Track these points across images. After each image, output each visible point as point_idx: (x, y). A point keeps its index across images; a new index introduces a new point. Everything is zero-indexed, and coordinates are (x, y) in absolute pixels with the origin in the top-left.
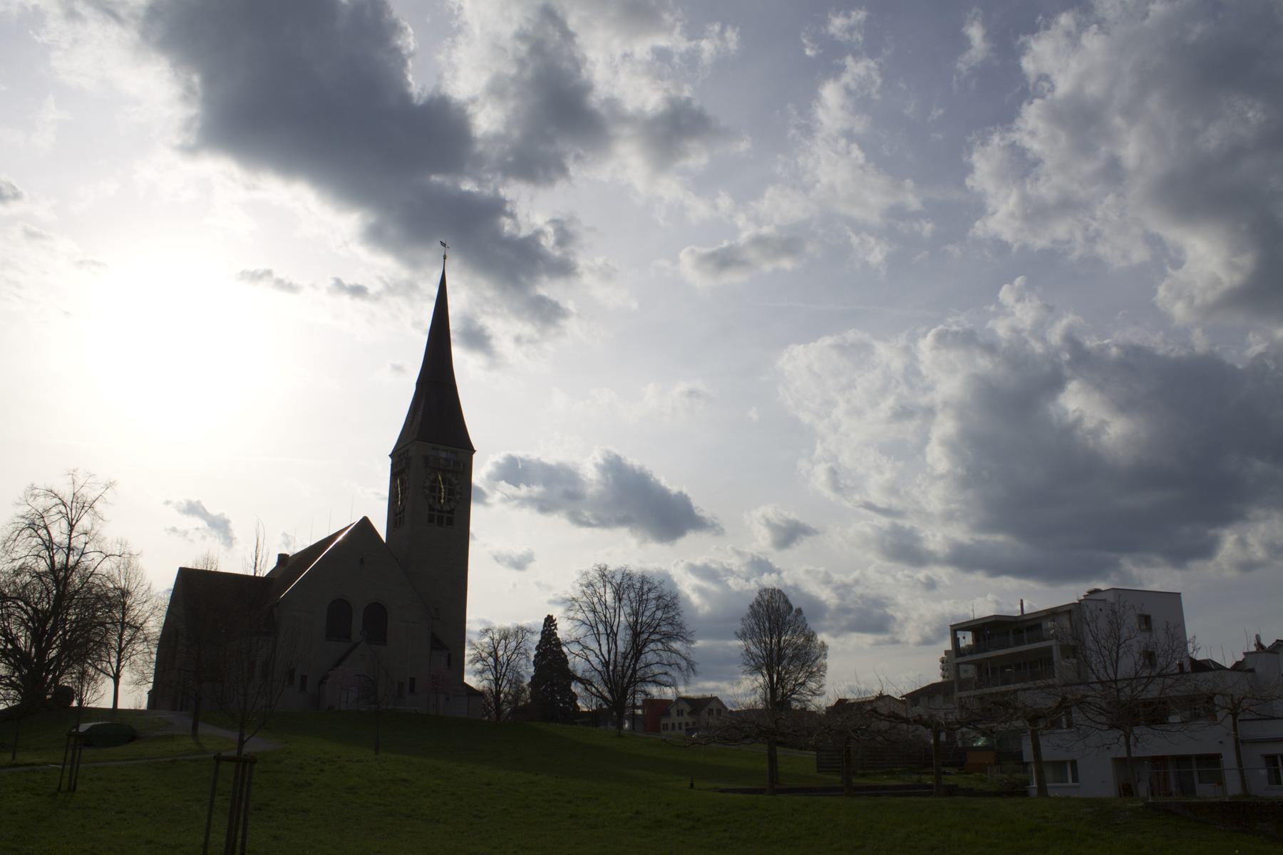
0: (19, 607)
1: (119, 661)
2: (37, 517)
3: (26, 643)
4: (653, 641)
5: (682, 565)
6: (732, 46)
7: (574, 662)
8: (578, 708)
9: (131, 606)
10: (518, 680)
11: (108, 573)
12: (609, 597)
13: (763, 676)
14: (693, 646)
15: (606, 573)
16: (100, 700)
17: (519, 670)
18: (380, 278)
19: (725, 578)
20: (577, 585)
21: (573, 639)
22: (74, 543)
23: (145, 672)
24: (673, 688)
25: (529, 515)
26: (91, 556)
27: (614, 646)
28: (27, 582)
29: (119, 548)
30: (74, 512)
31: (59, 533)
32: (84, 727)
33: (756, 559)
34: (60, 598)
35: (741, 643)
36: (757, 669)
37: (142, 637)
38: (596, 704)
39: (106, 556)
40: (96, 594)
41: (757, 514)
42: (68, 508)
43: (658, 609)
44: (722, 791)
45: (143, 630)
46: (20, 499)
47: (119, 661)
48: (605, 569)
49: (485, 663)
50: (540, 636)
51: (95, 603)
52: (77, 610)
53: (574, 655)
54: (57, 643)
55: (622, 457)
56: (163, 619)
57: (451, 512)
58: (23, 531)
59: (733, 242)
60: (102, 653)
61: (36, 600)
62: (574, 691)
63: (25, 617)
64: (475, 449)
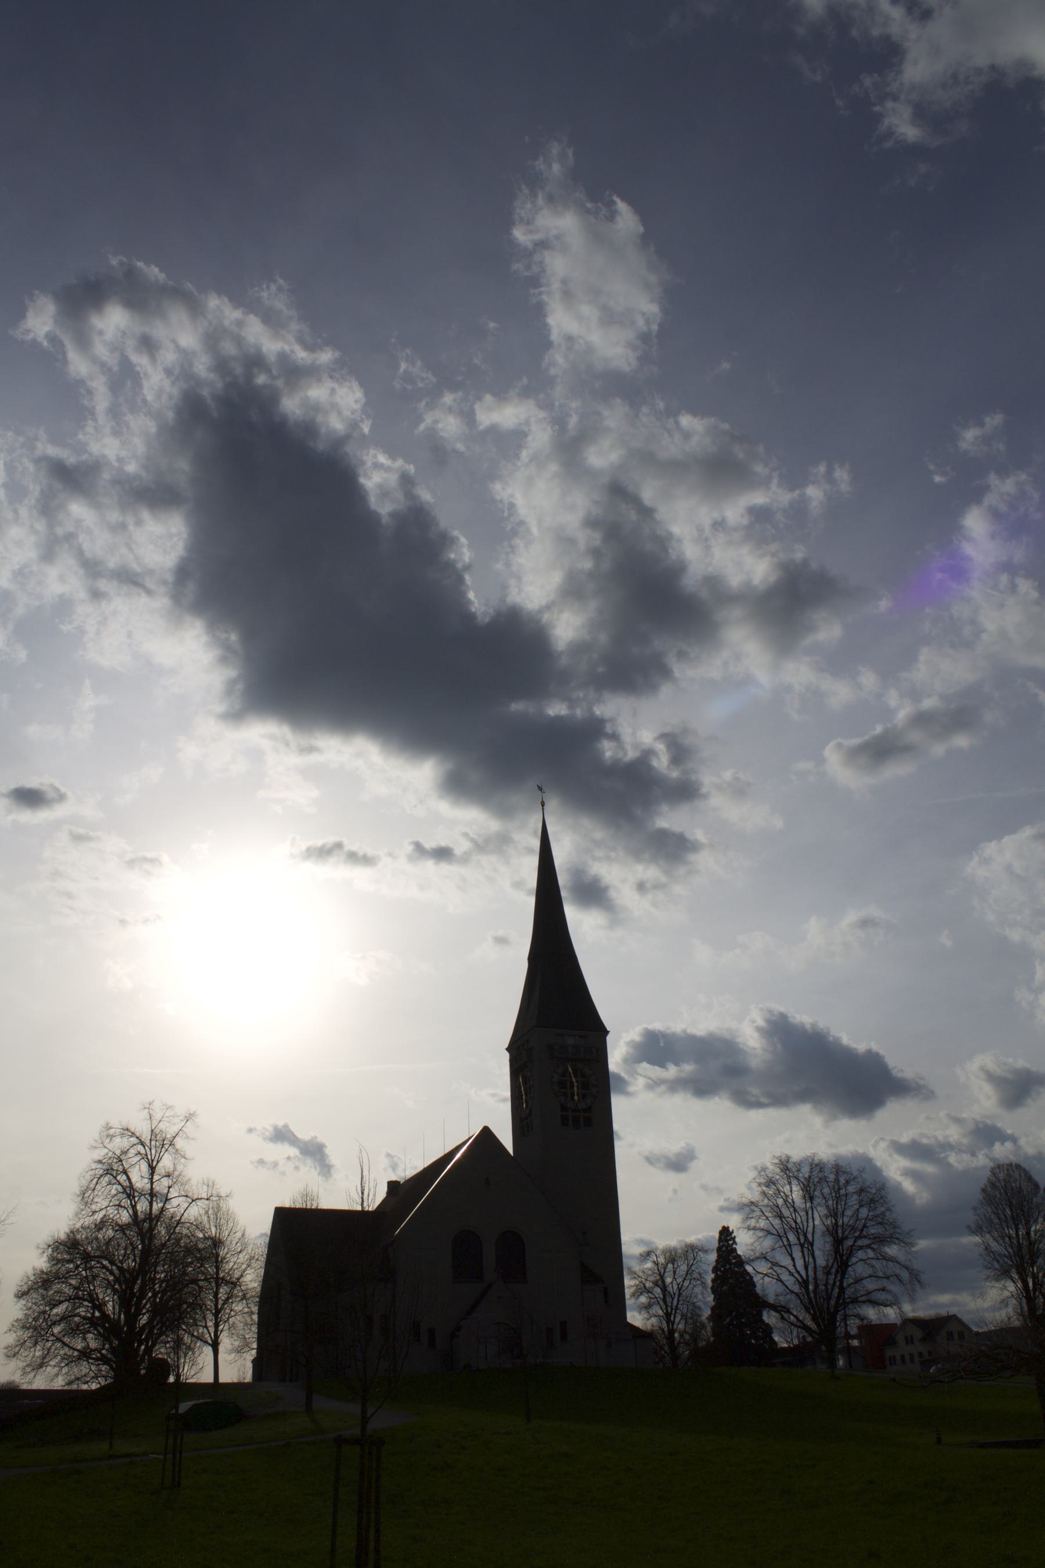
0: (104, 1267)
1: (217, 1325)
2: (115, 1160)
3: (114, 1308)
4: (861, 1248)
5: (883, 1145)
6: (844, 487)
7: (763, 1283)
8: (775, 1343)
9: (225, 1258)
10: (692, 1316)
11: (196, 1220)
12: (796, 1194)
13: (1014, 1282)
14: (913, 1249)
15: (790, 1166)
16: (200, 1374)
17: (695, 1300)
18: (466, 835)
19: (943, 1155)
20: (754, 1185)
21: (758, 1254)
22: (157, 1187)
23: (247, 1336)
24: (895, 1307)
25: (683, 1102)
26: (175, 1202)
27: (811, 1260)
28: (110, 1237)
29: (206, 1190)
30: (153, 1152)
31: (139, 1176)
32: (184, 1407)
33: (981, 1125)
34: (146, 1253)
35: (977, 1239)
36: (1004, 1273)
37: (240, 1294)
38: (798, 1337)
39: (193, 1201)
40: (186, 1246)
41: (974, 1065)
42: (146, 1147)
43: (861, 1206)
44: (983, 1446)
45: (240, 1286)
46: (96, 1141)
47: (217, 1325)
48: (788, 1161)
49: (650, 1295)
50: (716, 1255)
51: (185, 1257)
52: (166, 1267)
53: (762, 1276)
54: (147, 1307)
55: (789, 1015)
56: (262, 1272)
58: (102, 1179)
59: (889, 725)
60: (197, 1316)
61: (121, 1258)
62: (767, 1322)
63: (111, 1278)
64: (608, 1030)
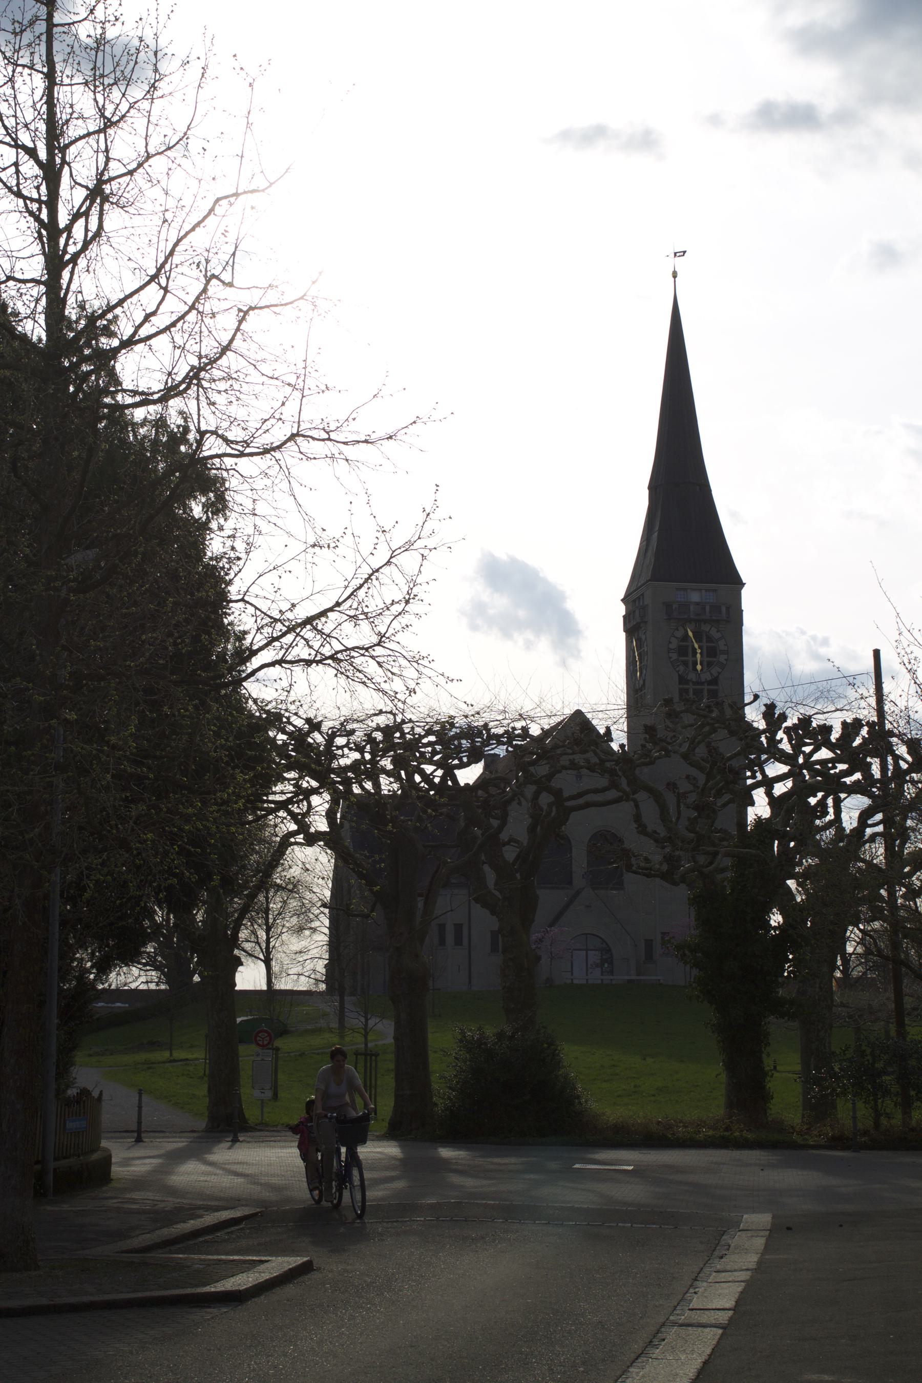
57: (714, 681)
